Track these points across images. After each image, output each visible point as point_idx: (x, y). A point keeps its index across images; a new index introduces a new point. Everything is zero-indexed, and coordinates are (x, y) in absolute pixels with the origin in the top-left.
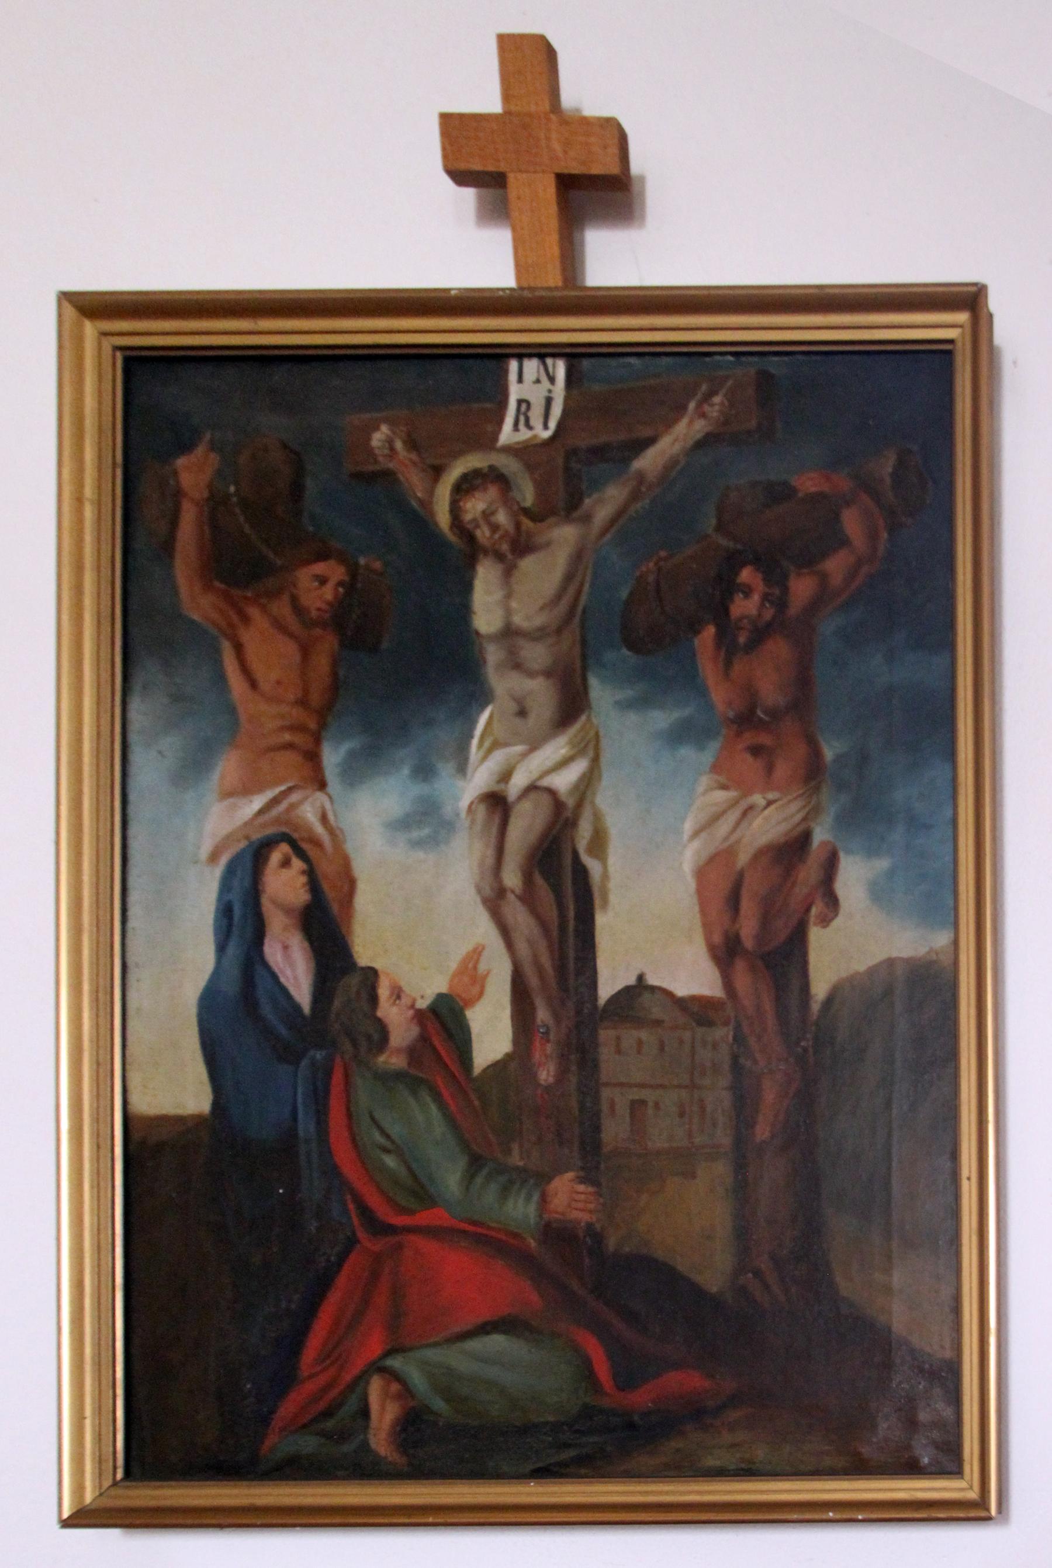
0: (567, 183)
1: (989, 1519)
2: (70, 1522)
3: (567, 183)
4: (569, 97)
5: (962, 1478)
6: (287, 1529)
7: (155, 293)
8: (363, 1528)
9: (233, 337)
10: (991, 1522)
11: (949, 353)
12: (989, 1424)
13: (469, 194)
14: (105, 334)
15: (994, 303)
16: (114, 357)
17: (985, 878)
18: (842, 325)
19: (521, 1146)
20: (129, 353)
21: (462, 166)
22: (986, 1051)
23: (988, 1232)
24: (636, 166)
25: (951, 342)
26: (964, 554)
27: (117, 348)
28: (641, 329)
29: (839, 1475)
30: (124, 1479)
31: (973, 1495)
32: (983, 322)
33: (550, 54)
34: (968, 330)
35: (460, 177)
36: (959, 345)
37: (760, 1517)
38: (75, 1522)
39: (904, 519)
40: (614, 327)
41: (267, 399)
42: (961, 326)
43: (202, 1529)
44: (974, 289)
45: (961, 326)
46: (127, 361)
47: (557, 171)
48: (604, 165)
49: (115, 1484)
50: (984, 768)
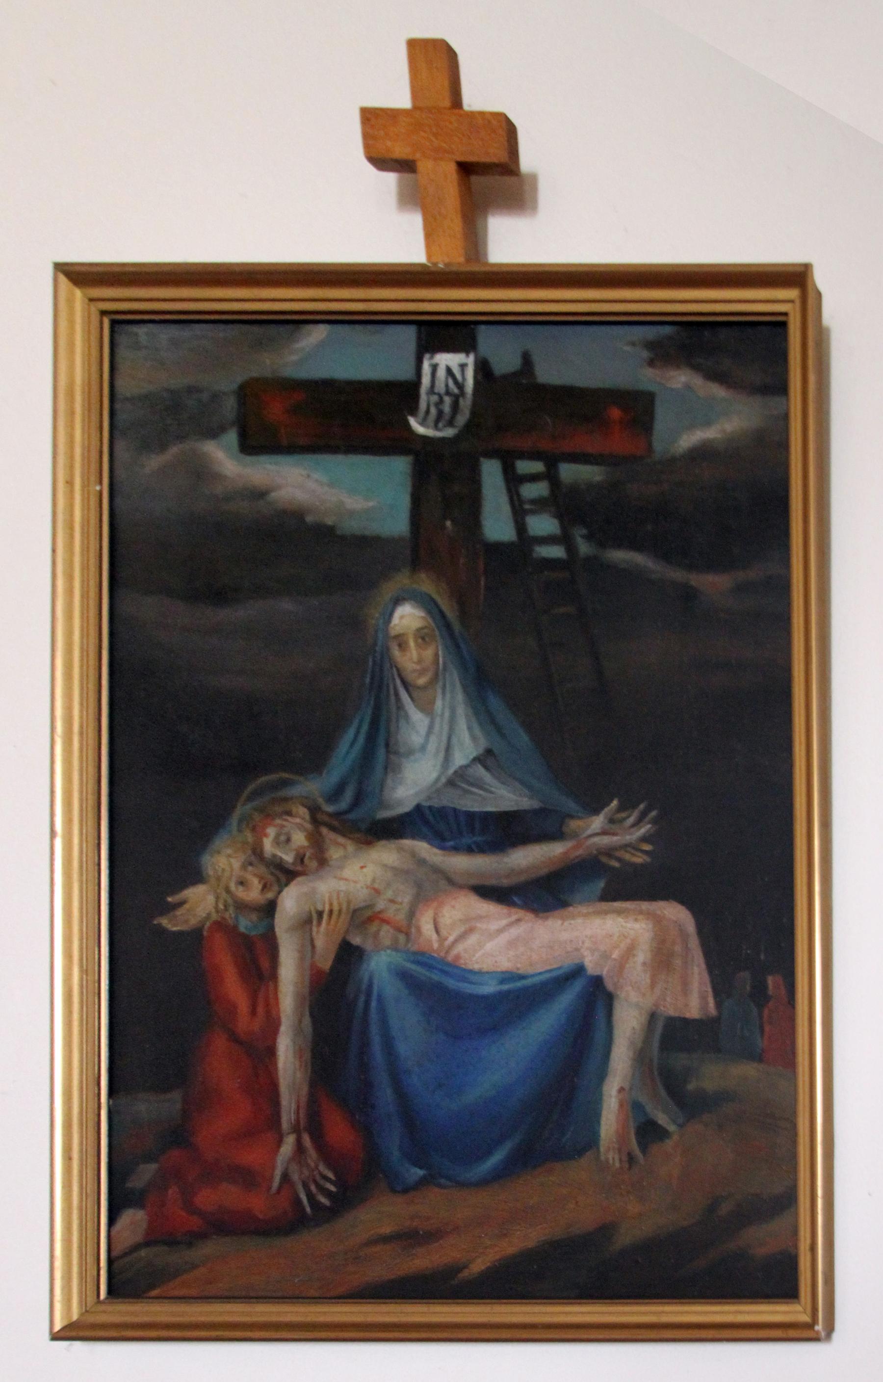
0: (466, 169)
2: (62, 1334)
3: (466, 169)
5: (799, 1303)
7: (165, 264)
9: (143, 303)
11: (783, 325)
12: (816, 1132)
13: (390, 179)
14: (91, 300)
15: (821, 279)
16: (101, 323)
17: (812, 702)
18: (683, 300)
22: (813, 815)
24: (527, 161)
25: (786, 314)
26: (695, 1313)
27: (103, 313)
28: (164, 300)
29: (783, 587)
30: (106, 1298)
31: (806, 1318)
32: (811, 301)
33: (451, 56)
35: (380, 162)
39: (446, 1163)
40: (415, 298)
44: (803, 269)
46: (114, 323)
47: (459, 159)
48: (496, 154)
49: (98, 1301)
50: (811, 610)
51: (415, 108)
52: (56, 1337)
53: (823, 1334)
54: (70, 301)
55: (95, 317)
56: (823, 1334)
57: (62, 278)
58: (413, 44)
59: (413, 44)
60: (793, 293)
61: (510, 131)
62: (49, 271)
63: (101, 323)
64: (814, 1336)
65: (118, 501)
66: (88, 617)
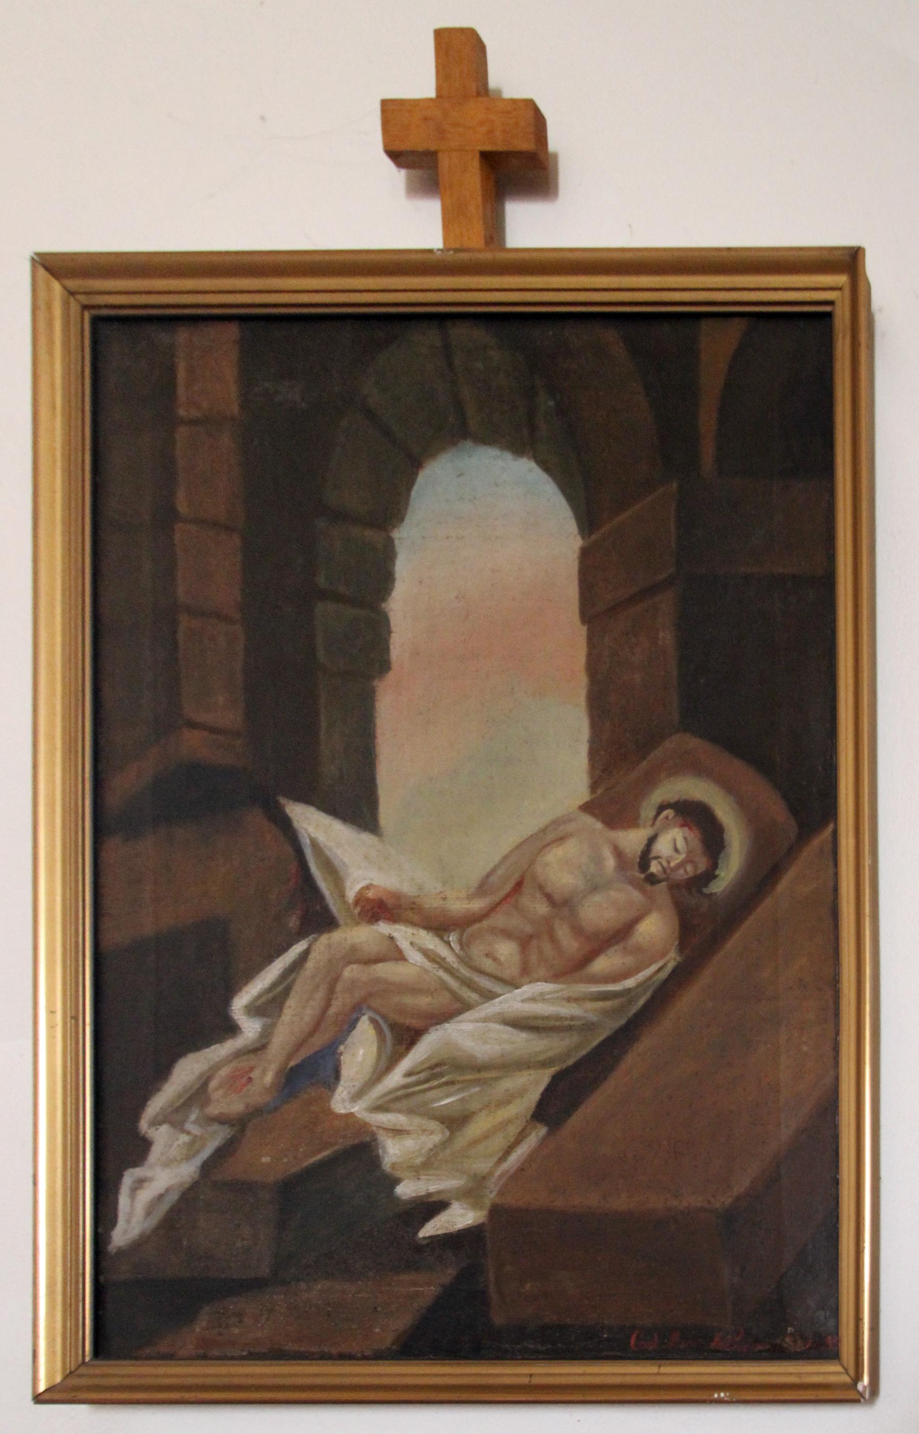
1: (856, 1401)
2: (47, 1396)
4: (495, 79)
6: (684, 1405)
8: (239, 1406)
10: (859, 1404)
11: (827, 317)
15: (873, 268)
16: (82, 315)
19: (544, 1139)
20: (95, 312)
21: (399, 146)
23: (864, 1226)
25: (830, 303)
27: (85, 307)
30: (91, 1360)
31: (846, 1379)
34: (847, 291)
35: (396, 156)
36: (838, 305)
37: (517, 1398)
38: (56, 1396)
41: (808, 1276)
42: (840, 289)
43: (693, 1405)
45: (840, 289)
46: (97, 321)
48: (526, 145)
49: (84, 1362)
51: (439, 95)
52: (39, 1399)
53: (867, 1395)
54: (49, 289)
55: (75, 308)
56: (867, 1395)
57: (41, 272)
58: (439, 34)
59: (439, 34)
60: (842, 279)
61: (539, 122)
62: (27, 267)
63: (82, 315)
64: (857, 1397)
65: (106, 923)
66: (70, 865)
